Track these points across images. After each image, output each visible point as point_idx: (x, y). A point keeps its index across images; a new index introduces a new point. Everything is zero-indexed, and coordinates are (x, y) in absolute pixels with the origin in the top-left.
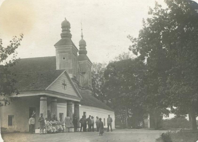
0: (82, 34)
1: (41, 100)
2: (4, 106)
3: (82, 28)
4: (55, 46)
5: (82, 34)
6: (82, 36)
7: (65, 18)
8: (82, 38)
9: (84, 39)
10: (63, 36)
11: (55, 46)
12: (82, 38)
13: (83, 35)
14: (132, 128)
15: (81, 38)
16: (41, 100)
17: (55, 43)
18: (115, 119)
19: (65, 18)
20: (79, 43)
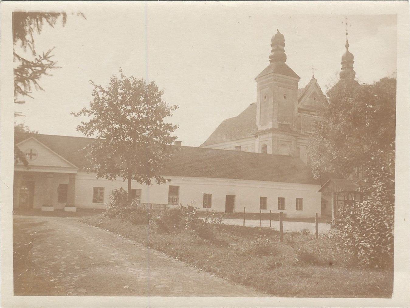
0: (347, 41)
1: (260, 221)
2: (94, 89)
3: (348, 32)
4: (255, 79)
5: (347, 41)
6: (347, 46)
7: (278, 30)
8: (347, 49)
9: (350, 50)
10: (273, 59)
11: (255, 79)
12: (347, 49)
13: (349, 44)
14: (94, 209)
15: (344, 51)
16: (260, 221)
17: (255, 76)
18: (331, 298)
19: (278, 30)
20: (272, 40)
